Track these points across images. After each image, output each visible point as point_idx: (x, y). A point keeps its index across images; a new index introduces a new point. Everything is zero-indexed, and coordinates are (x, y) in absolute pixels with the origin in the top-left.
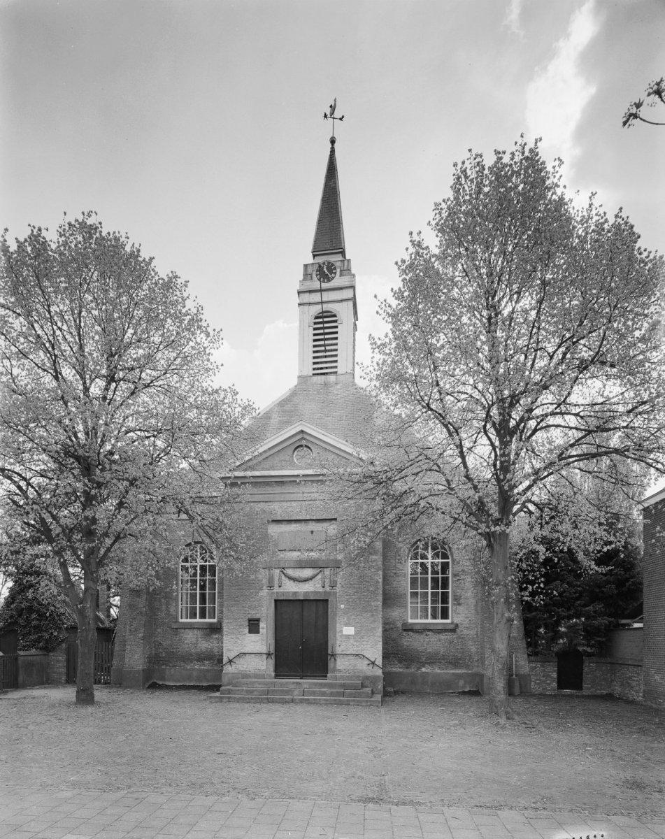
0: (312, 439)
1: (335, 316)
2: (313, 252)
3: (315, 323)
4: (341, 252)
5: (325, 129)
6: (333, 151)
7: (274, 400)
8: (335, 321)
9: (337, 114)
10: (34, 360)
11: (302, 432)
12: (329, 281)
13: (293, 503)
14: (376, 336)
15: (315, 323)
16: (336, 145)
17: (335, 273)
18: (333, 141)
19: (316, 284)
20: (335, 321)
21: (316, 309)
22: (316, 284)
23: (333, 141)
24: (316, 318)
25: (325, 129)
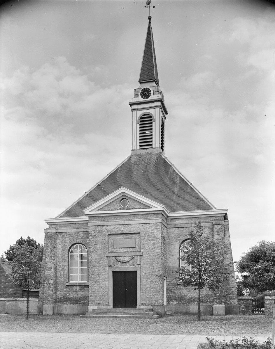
0: (128, 196)
1: (151, 117)
2: (139, 81)
3: (141, 121)
4: (155, 81)
5: (146, 12)
6: (149, 28)
7: (75, 201)
8: (151, 120)
9: (151, 5)
10: (102, 227)
11: (123, 192)
12: (147, 98)
13: (136, 241)
14: (22, 238)
15: (141, 121)
16: (151, 20)
17: (150, 94)
18: (150, 19)
19: (140, 99)
20: (151, 120)
21: (140, 113)
22: (140, 99)
23: (150, 19)
24: (141, 118)
25: (146, 12)
